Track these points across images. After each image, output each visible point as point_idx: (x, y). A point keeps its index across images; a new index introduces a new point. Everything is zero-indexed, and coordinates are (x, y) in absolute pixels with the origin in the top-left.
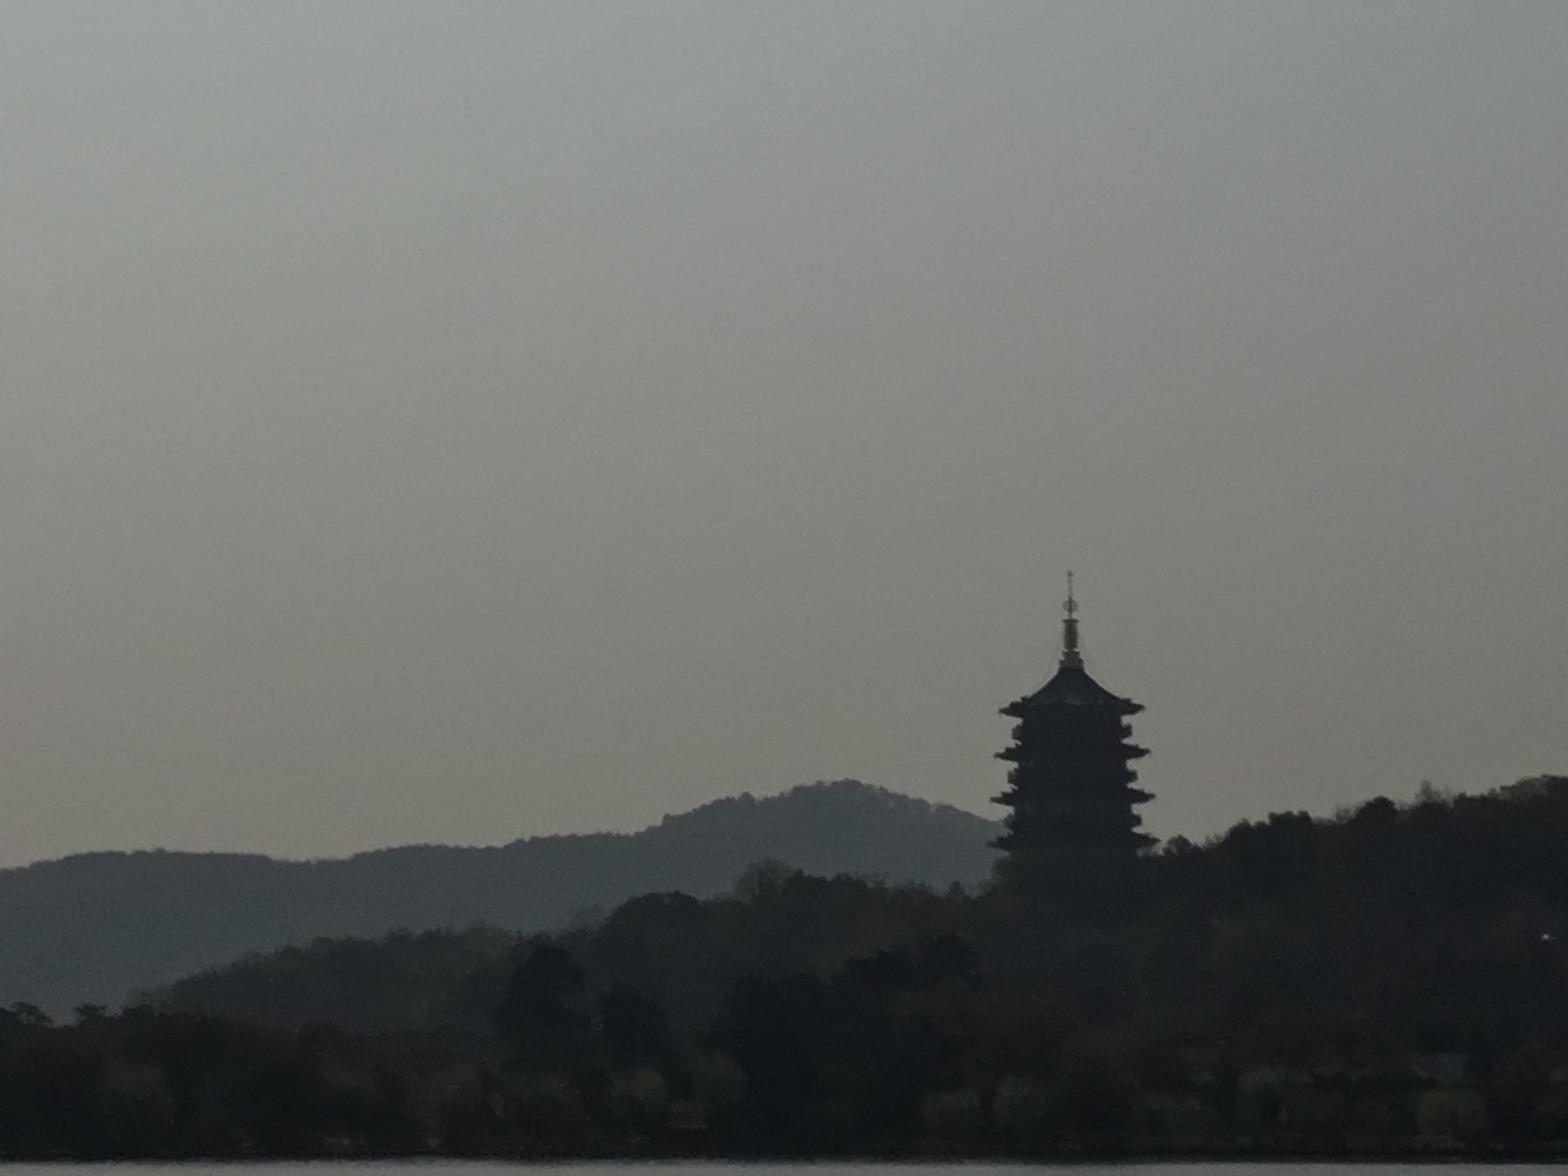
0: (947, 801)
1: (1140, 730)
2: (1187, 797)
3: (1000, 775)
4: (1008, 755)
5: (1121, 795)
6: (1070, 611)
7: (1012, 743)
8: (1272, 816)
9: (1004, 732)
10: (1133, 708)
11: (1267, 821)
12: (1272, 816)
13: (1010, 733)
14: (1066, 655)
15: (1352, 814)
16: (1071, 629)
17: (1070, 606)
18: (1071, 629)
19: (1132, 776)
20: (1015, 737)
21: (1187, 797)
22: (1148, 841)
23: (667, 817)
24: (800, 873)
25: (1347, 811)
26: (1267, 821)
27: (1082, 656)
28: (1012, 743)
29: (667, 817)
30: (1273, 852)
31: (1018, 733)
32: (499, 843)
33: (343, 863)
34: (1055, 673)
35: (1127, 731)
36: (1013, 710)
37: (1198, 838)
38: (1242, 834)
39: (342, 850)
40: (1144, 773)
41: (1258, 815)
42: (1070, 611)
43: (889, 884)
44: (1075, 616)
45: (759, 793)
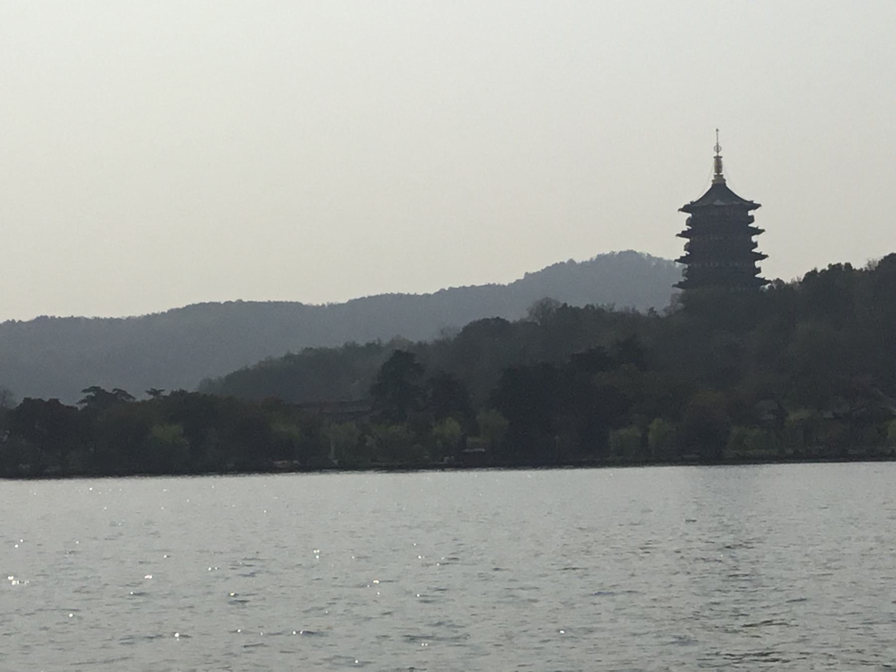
0: (169, 308)
1: (759, 218)
2: (783, 259)
3: (677, 249)
4: (684, 234)
5: (752, 257)
6: (718, 152)
7: (686, 228)
8: (830, 265)
9: (681, 222)
10: (756, 206)
11: (827, 269)
12: (830, 265)
13: (685, 223)
14: (715, 176)
15: (877, 264)
16: (718, 159)
17: (718, 149)
18: (718, 159)
19: (755, 245)
20: (685, 250)
21: (783, 259)
22: (763, 281)
23: (527, 274)
24: (565, 304)
25: (874, 262)
26: (827, 269)
27: (725, 177)
28: (686, 228)
29: (527, 274)
30: (831, 286)
31: (689, 222)
32: (432, 292)
33: (343, 304)
34: (709, 187)
35: (752, 219)
36: (685, 209)
37: (787, 280)
38: (812, 275)
39: (432, 290)
40: (762, 244)
41: (822, 266)
42: (718, 152)
43: (617, 309)
44: (720, 154)
45: (578, 260)
